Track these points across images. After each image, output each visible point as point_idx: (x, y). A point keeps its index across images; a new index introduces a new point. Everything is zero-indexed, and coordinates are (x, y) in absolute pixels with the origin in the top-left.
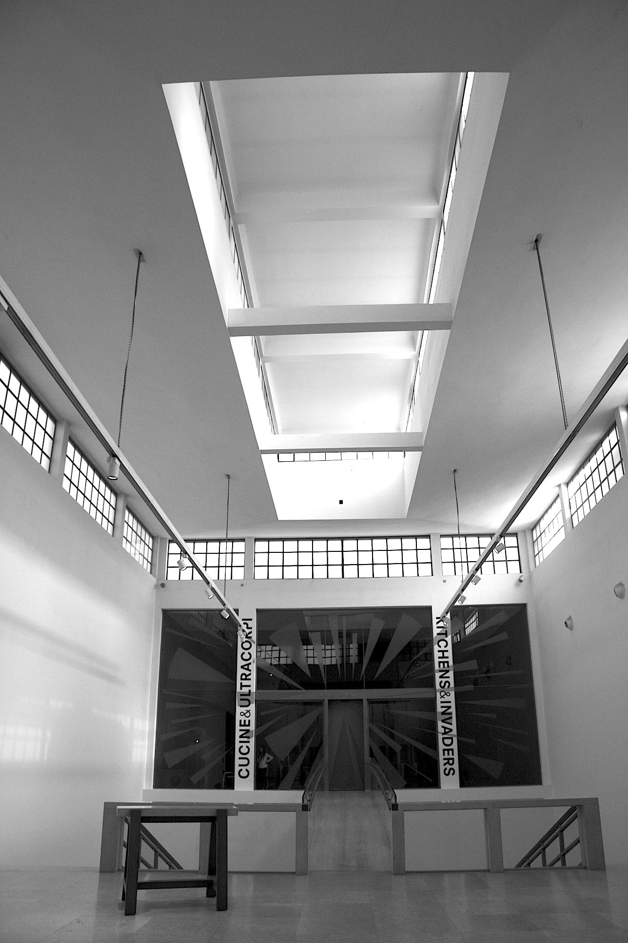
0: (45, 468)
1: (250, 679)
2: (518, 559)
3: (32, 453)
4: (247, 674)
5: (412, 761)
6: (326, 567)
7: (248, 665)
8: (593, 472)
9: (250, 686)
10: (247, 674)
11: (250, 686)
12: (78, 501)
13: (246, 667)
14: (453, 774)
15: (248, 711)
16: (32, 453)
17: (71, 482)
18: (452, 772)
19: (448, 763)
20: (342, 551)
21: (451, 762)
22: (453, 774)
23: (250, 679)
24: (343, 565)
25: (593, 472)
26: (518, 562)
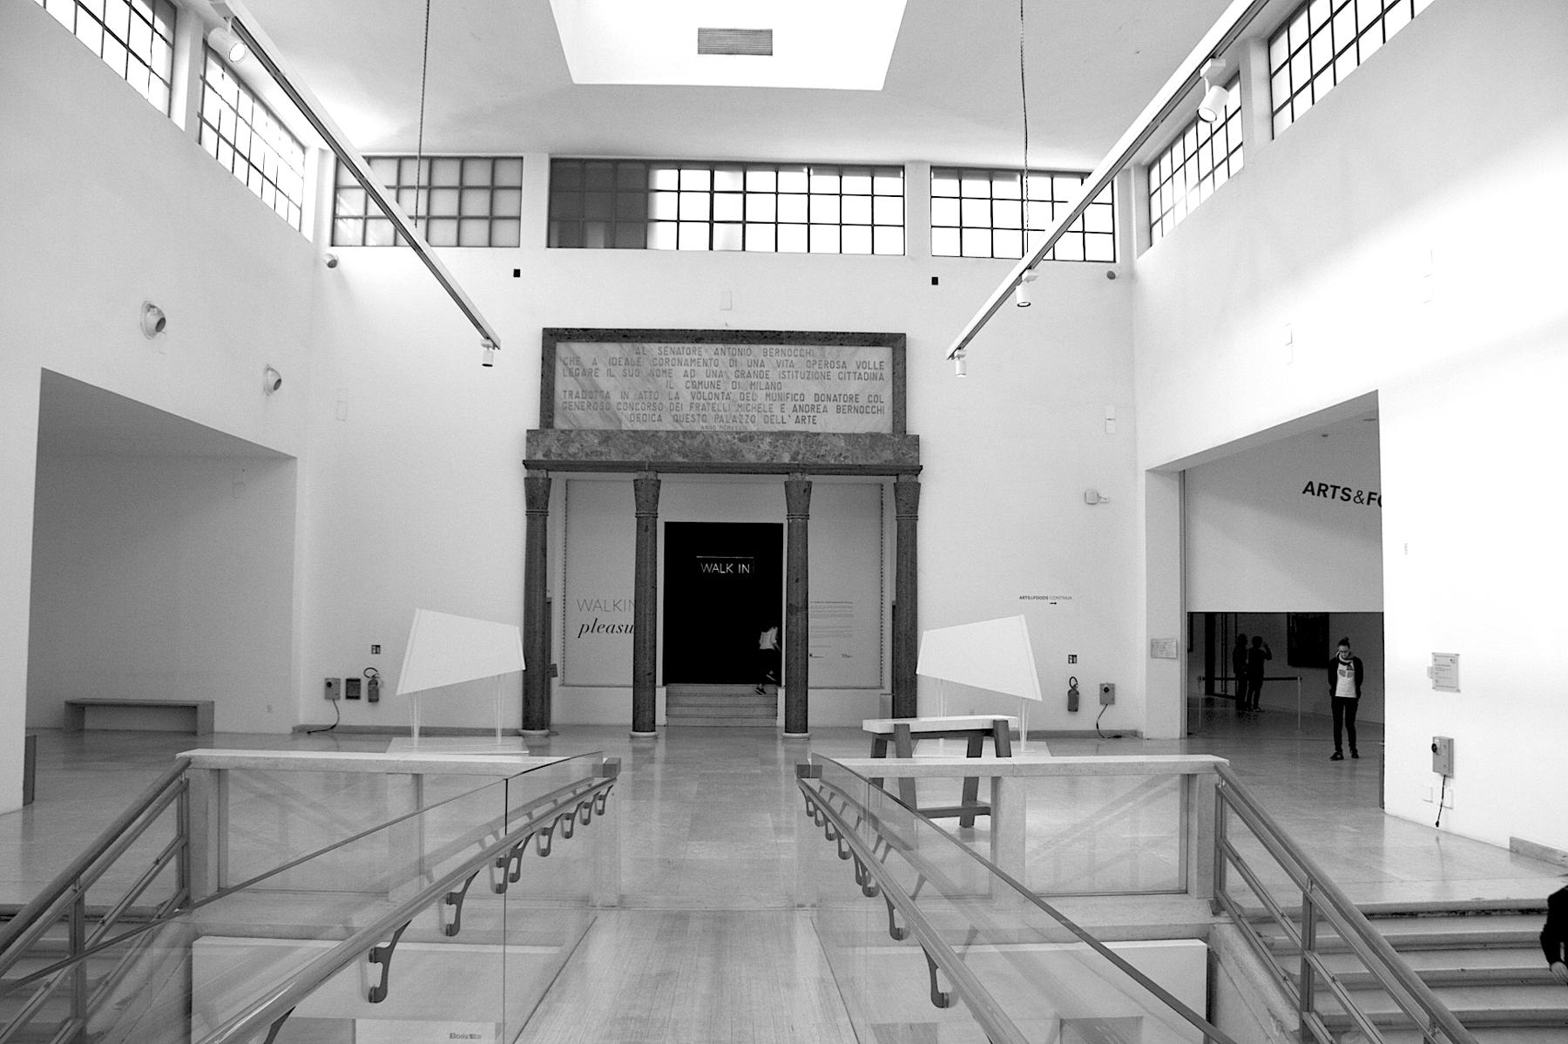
0: (161, 110)
1: (1318, 495)
2: (1111, 202)
3: (75, 30)
4: (1327, 493)
5: (644, 647)
6: (843, 227)
7: (1312, 491)
8: (1202, 146)
9: (1333, 497)
10: (1327, 493)
11: (1333, 497)
12: (289, 222)
13: (1310, 488)
14: (1350, 491)
15: (1361, 502)
16: (75, 30)
17: (220, 136)
18: (1346, 491)
19: (1324, 491)
20: (961, 228)
21: (1323, 488)
22: (1350, 491)
23: (1318, 495)
24: (809, 194)
25: (1202, 146)
26: (1111, 206)
